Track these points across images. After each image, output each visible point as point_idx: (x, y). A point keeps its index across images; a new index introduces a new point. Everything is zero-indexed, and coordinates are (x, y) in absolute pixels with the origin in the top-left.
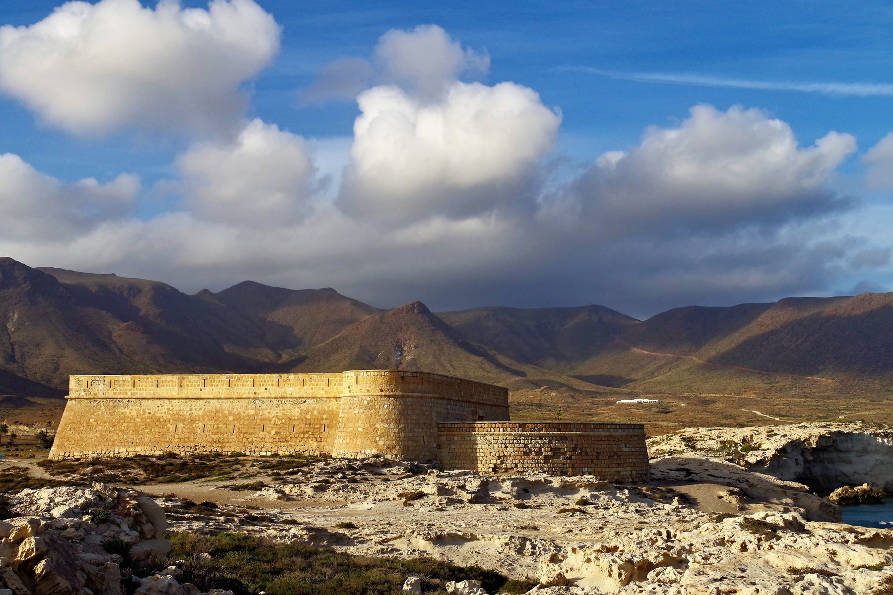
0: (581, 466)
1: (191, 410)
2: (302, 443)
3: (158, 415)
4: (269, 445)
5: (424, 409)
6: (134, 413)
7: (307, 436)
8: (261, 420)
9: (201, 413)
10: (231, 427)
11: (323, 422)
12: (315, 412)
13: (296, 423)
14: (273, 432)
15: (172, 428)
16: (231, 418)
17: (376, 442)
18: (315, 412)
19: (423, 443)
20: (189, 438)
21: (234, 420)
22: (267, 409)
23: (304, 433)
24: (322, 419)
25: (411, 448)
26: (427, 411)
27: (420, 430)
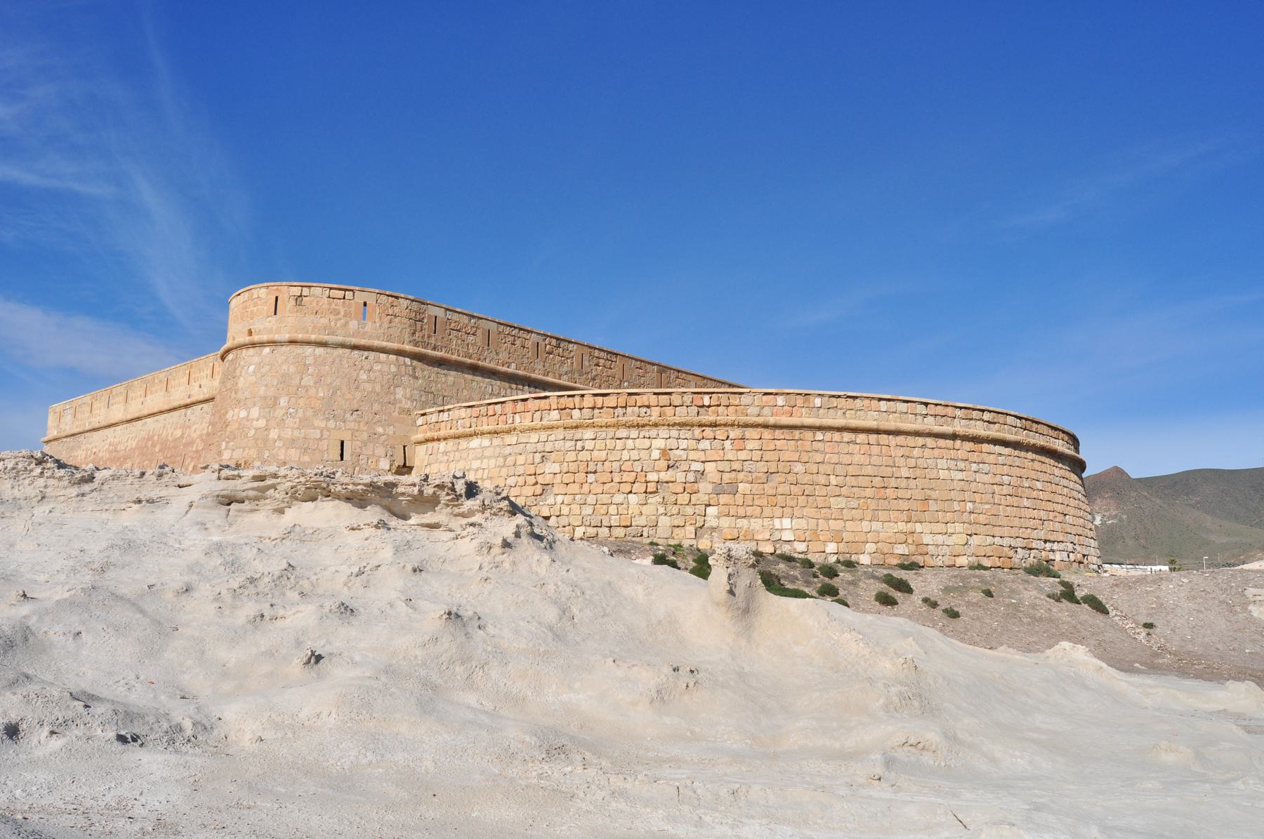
0: (767, 512)
5: (364, 376)
26: (369, 381)
27: (332, 424)
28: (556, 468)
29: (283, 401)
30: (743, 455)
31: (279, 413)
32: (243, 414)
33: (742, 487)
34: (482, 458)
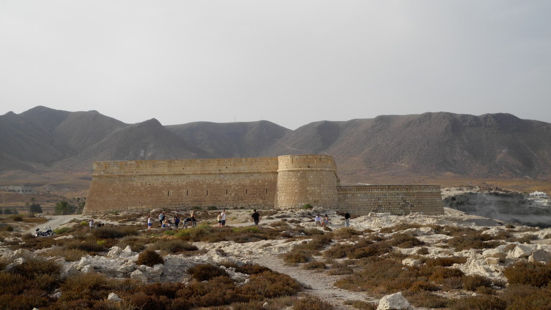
1: (178, 181)
2: (252, 200)
3: (156, 185)
4: (231, 202)
6: (139, 184)
7: (255, 196)
8: (225, 187)
9: (184, 183)
10: (205, 192)
11: (266, 187)
12: (260, 181)
13: (248, 188)
14: (233, 194)
15: (166, 193)
16: (205, 186)
17: (307, 198)
18: (260, 181)
19: (333, 199)
20: (177, 199)
21: (207, 187)
22: (228, 180)
23: (254, 194)
24: (265, 185)
25: (327, 201)
28: (382, 202)
29: (322, 185)
30: (414, 199)
31: (322, 188)
32: (313, 188)
33: (415, 206)
34: (362, 199)
